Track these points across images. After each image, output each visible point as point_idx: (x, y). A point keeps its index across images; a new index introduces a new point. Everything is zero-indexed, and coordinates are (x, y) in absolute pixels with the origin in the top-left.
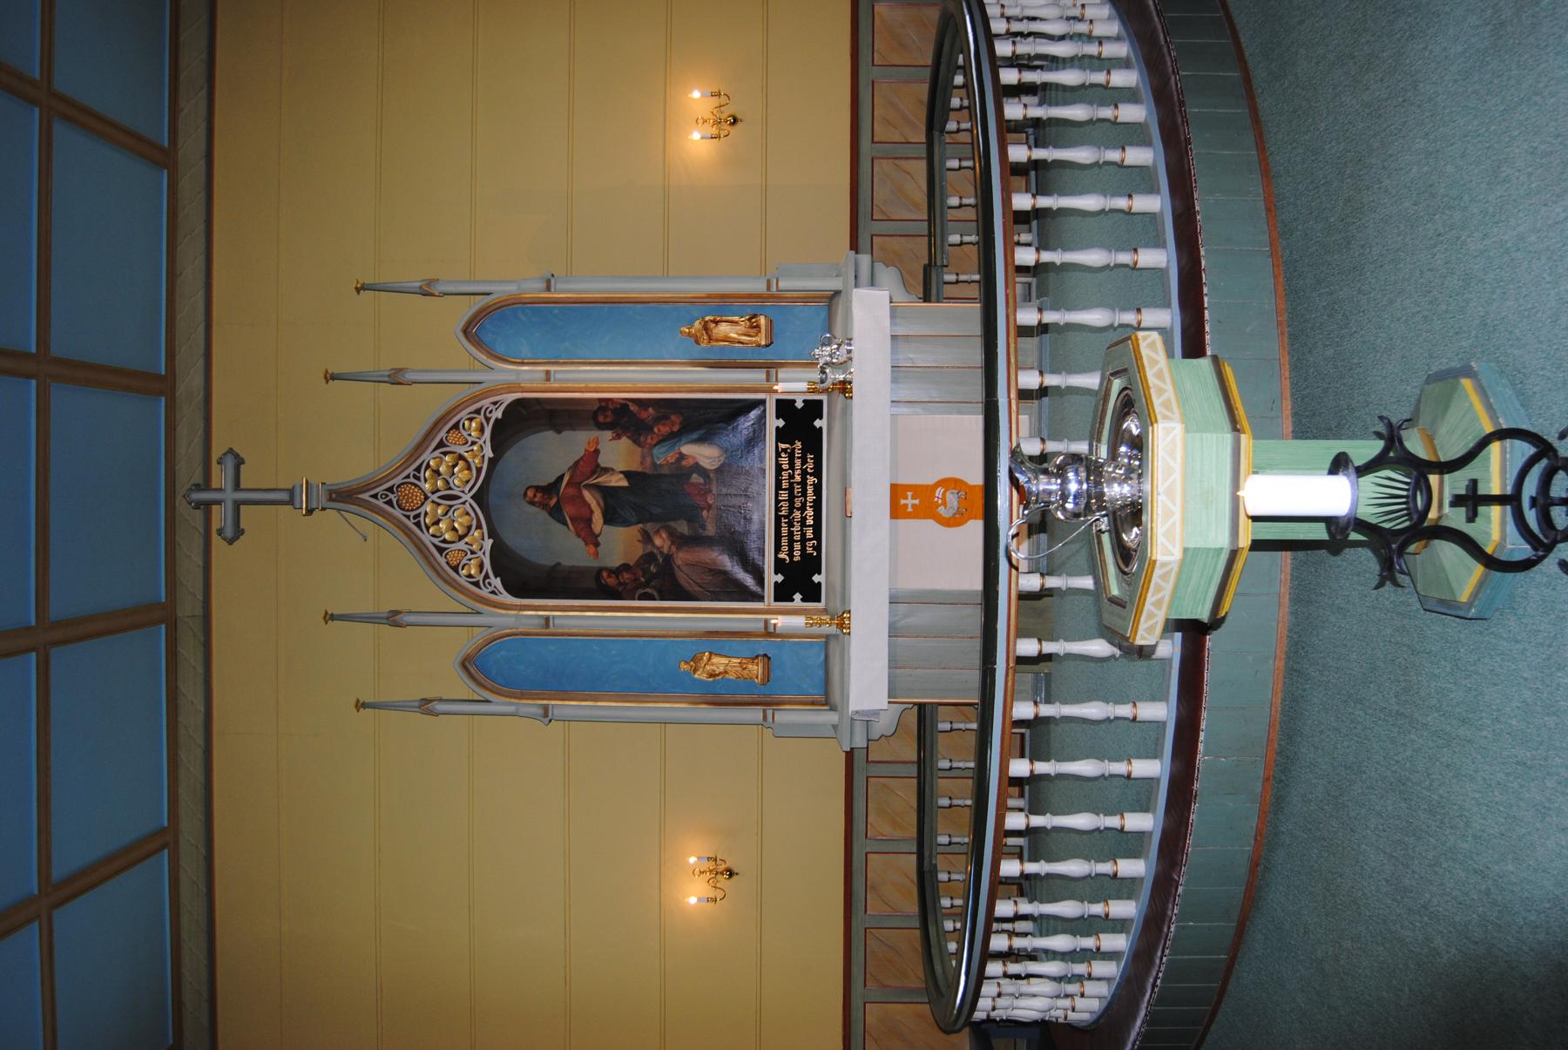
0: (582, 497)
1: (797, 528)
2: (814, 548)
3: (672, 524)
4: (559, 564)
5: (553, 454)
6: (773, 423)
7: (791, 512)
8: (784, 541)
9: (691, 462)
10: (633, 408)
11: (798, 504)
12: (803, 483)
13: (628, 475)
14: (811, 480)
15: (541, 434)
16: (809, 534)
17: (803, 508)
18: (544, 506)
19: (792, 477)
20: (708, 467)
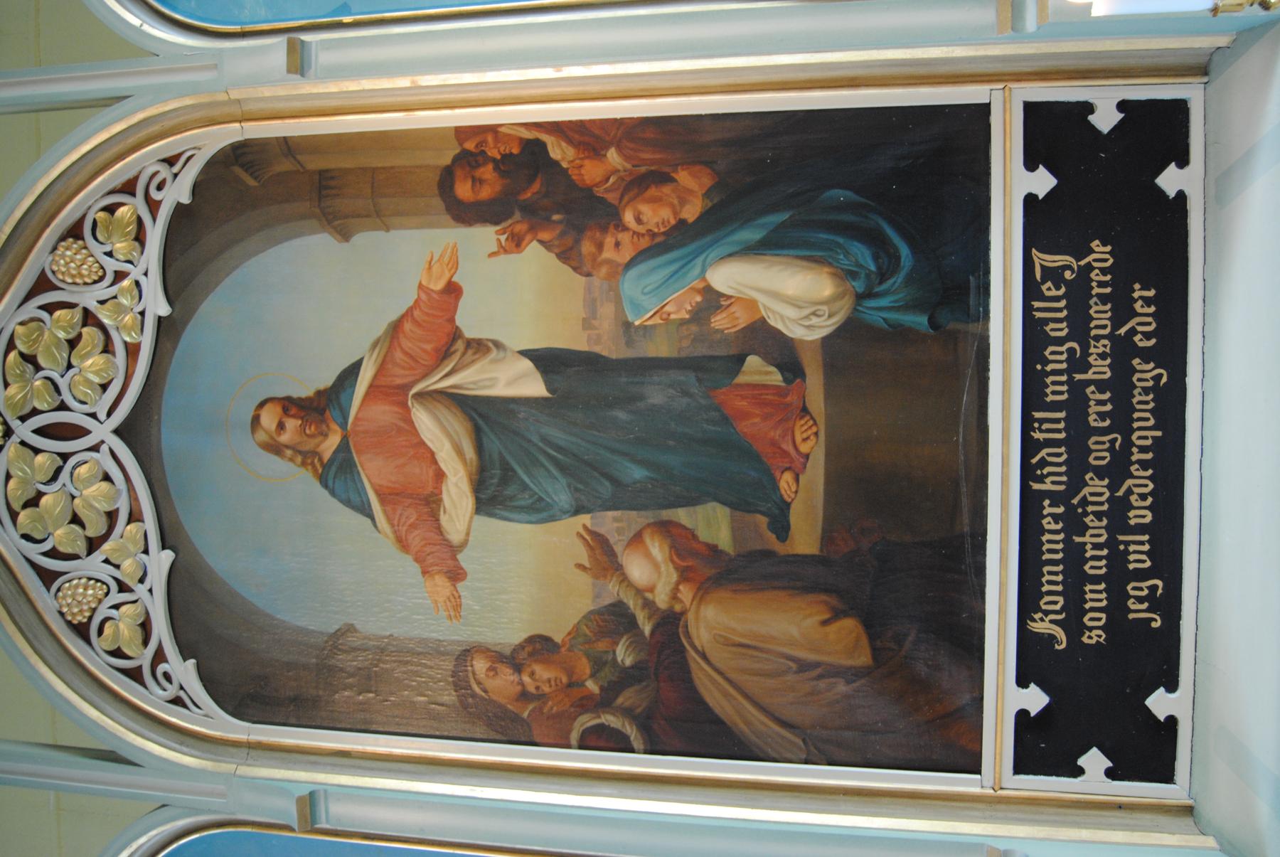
0: (414, 431)
1: (1095, 533)
2: (1153, 601)
3: (682, 515)
4: (350, 629)
5: (322, 302)
6: (1014, 183)
7: (1076, 483)
8: (1052, 578)
9: (742, 319)
10: (558, 151)
11: (1100, 454)
12: (1120, 385)
13: (546, 361)
14: (1146, 373)
15: (297, 242)
16: (1139, 558)
17: (1117, 470)
18: (307, 457)
19: (1078, 363)
20: (795, 332)
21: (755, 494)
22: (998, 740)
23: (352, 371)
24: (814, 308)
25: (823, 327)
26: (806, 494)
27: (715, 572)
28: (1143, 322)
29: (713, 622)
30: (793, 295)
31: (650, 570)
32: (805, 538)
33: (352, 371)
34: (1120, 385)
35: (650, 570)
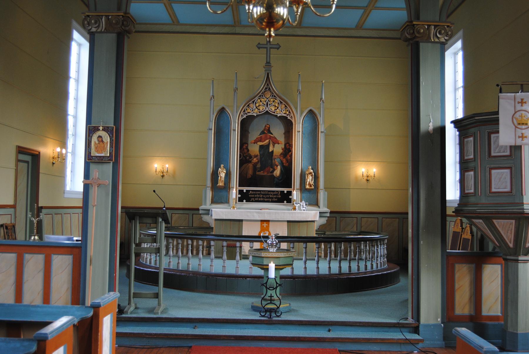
1: (258, 196)
5: (278, 132)
6: (285, 190)
8: (254, 193)
11: (264, 196)
12: (269, 198)
13: (273, 152)
14: (270, 200)
16: (256, 199)
17: (263, 197)
18: (265, 129)
19: (271, 195)
21: (262, 169)
22: (241, 188)
23: (272, 134)
24: (276, 174)
25: (275, 175)
26: (261, 173)
27: (255, 165)
28: (274, 200)
29: (250, 165)
30: (277, 172)
31: (255, 160)
32: (258, 173)
33: (272, 134)
34: (269, 198)
35: (255, 160)
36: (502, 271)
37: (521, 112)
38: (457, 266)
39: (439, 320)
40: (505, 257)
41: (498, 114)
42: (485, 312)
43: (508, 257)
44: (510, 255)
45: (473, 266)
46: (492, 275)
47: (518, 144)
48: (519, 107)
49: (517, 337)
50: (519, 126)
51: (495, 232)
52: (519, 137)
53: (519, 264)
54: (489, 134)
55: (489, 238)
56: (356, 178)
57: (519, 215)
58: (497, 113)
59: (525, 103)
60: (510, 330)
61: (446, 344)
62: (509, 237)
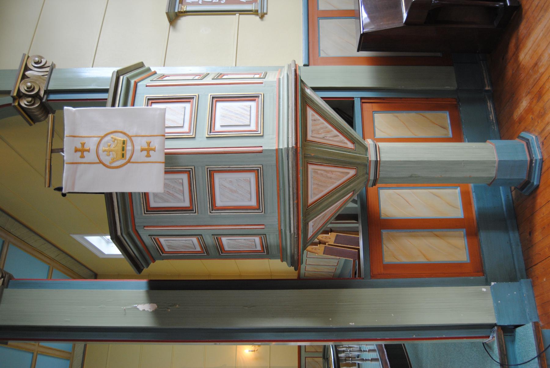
36: (389, 188)
37: (100, 152)
38: (388, 259)
39: (484, 290)
40: (371, 183)
41: (111, 194)
42: (459, 214)
43: (372, 177)
44: (368, 174)
45: (384, 233)
46: (393, 203)
47: (162, 159)
48: (91, 157)
49: (502, 161)
50: (128, 156)
51: (330, 200)
52: (148, 156)
53: (383, 159)
54: (149, 210)
55: (340, 207)
56: (256, 359)
57: (300, 156)
58: (109, 196)
59: (83, 144)
60: (493, 173)
61: (522, 277)
62: (339, 176)
